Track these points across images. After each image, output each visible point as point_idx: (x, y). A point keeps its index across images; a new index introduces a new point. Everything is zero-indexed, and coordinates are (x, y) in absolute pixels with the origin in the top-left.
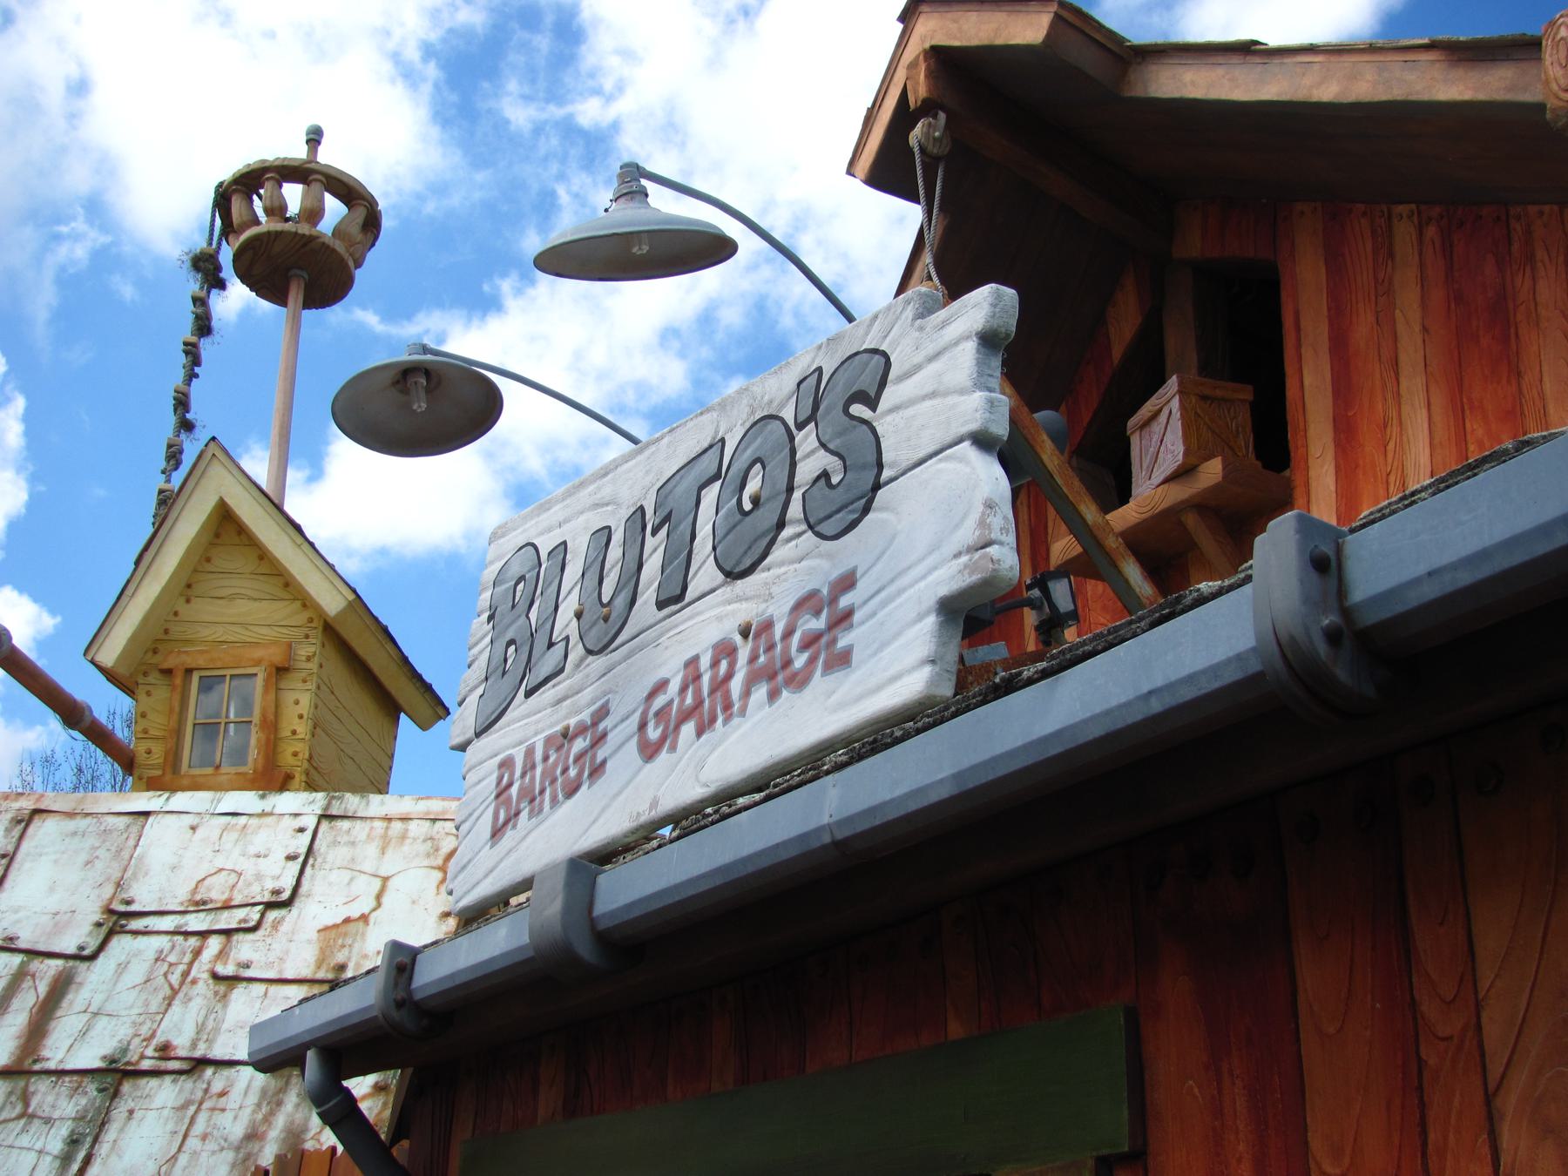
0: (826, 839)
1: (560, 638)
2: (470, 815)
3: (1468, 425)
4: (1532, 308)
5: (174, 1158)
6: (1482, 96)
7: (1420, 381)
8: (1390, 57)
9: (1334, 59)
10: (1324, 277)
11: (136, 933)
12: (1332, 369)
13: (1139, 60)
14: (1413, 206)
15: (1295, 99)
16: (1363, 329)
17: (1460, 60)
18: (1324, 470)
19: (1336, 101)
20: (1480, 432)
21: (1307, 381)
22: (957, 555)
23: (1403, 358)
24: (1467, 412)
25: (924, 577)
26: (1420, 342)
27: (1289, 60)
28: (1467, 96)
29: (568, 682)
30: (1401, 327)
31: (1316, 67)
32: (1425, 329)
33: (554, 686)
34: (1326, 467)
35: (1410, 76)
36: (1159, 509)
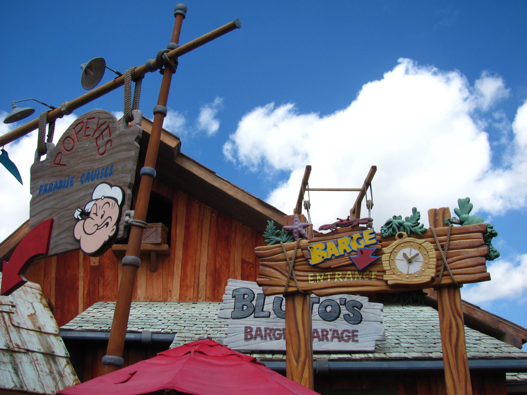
0: (385, 369)
1: (268, 311)
2: (233, 333)
3: (217, 258)
4: (234, 241)
5: (39, 376)
6: (264, 213)
7: (207, 244)
8: (246, 194)
9: (233, 187)
10: (185, 211)
11: (66, 325)
12: (185, 232)
13: (181, 156)
14: (210, 207)
15: (249, 205)
16: (194, 226)
17: (261, 204)
18: (179, 253)
19: (232, 195)
20: (219, 260)
21: (178, 232)
22: (380, 336)
23: (203, 238)
24: (217, 255)
25: (373, 336)
26: (208, 236)
27: (221, 180)
28: (261, 211)
29: (272, 320)
30: (204, 231)
31: (228, 186)
32: (209, 234)
33: (266, 319)
34: (180, 252)
35: (250, 201)
36: (148, 249)
